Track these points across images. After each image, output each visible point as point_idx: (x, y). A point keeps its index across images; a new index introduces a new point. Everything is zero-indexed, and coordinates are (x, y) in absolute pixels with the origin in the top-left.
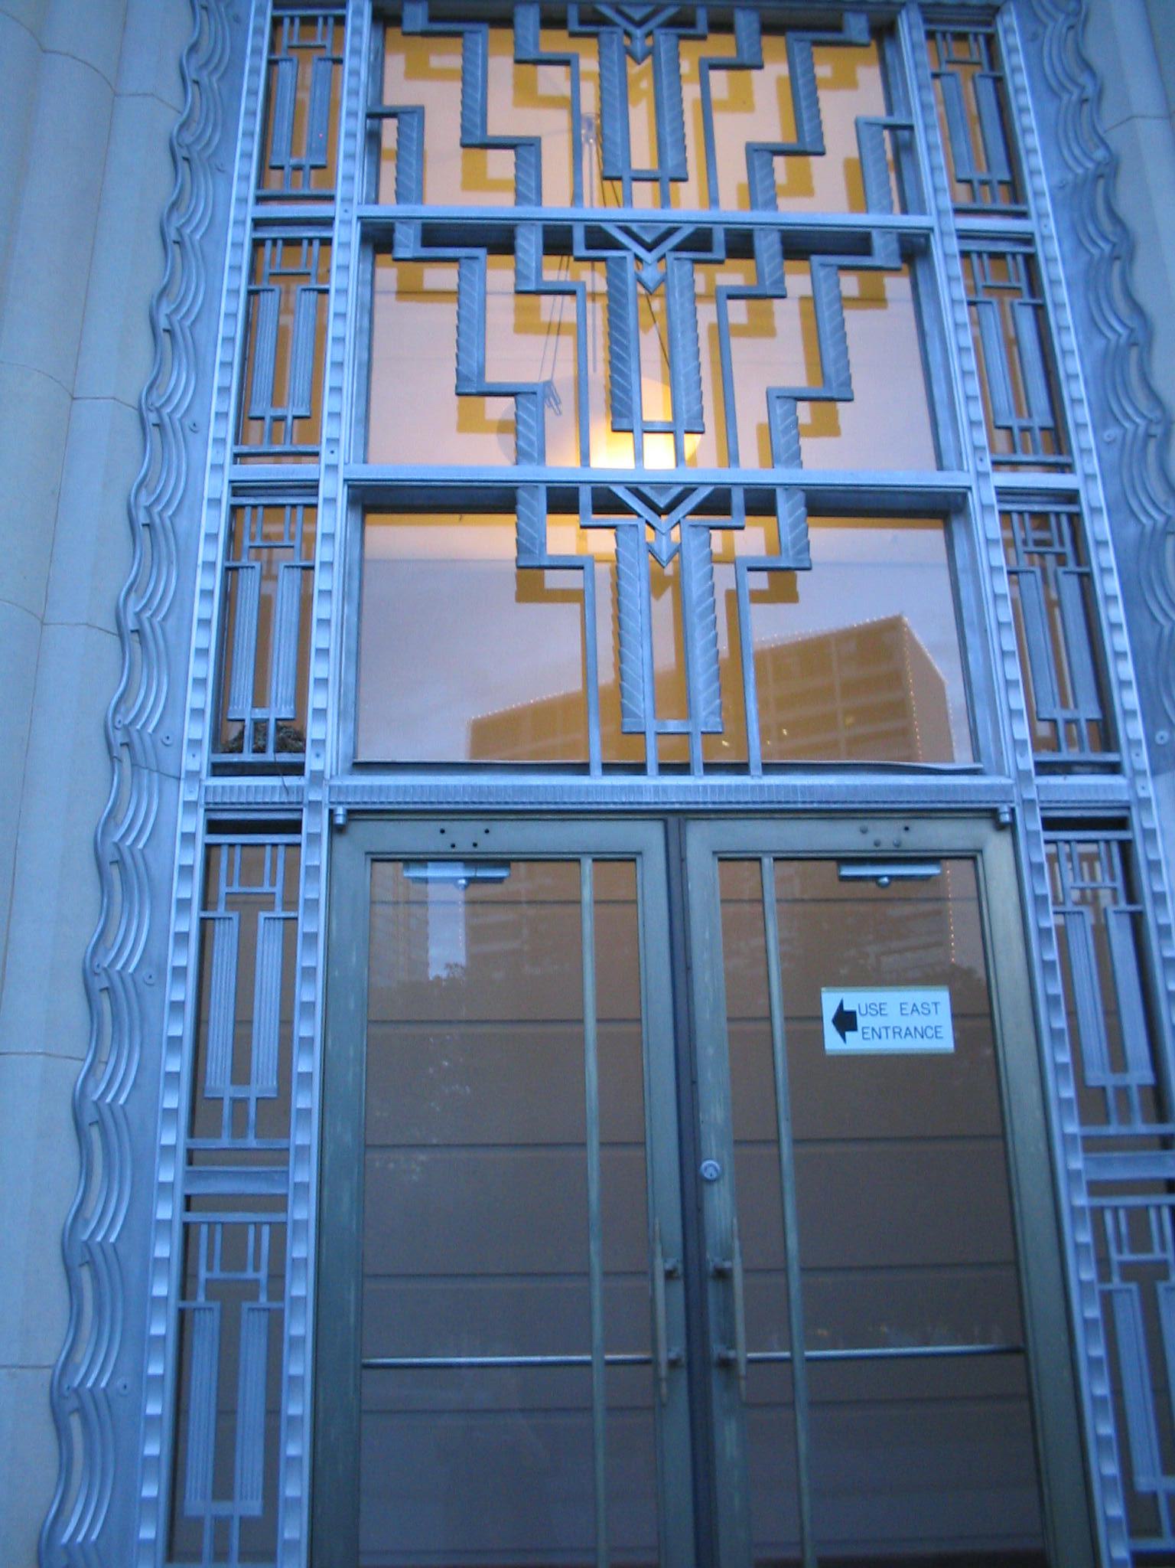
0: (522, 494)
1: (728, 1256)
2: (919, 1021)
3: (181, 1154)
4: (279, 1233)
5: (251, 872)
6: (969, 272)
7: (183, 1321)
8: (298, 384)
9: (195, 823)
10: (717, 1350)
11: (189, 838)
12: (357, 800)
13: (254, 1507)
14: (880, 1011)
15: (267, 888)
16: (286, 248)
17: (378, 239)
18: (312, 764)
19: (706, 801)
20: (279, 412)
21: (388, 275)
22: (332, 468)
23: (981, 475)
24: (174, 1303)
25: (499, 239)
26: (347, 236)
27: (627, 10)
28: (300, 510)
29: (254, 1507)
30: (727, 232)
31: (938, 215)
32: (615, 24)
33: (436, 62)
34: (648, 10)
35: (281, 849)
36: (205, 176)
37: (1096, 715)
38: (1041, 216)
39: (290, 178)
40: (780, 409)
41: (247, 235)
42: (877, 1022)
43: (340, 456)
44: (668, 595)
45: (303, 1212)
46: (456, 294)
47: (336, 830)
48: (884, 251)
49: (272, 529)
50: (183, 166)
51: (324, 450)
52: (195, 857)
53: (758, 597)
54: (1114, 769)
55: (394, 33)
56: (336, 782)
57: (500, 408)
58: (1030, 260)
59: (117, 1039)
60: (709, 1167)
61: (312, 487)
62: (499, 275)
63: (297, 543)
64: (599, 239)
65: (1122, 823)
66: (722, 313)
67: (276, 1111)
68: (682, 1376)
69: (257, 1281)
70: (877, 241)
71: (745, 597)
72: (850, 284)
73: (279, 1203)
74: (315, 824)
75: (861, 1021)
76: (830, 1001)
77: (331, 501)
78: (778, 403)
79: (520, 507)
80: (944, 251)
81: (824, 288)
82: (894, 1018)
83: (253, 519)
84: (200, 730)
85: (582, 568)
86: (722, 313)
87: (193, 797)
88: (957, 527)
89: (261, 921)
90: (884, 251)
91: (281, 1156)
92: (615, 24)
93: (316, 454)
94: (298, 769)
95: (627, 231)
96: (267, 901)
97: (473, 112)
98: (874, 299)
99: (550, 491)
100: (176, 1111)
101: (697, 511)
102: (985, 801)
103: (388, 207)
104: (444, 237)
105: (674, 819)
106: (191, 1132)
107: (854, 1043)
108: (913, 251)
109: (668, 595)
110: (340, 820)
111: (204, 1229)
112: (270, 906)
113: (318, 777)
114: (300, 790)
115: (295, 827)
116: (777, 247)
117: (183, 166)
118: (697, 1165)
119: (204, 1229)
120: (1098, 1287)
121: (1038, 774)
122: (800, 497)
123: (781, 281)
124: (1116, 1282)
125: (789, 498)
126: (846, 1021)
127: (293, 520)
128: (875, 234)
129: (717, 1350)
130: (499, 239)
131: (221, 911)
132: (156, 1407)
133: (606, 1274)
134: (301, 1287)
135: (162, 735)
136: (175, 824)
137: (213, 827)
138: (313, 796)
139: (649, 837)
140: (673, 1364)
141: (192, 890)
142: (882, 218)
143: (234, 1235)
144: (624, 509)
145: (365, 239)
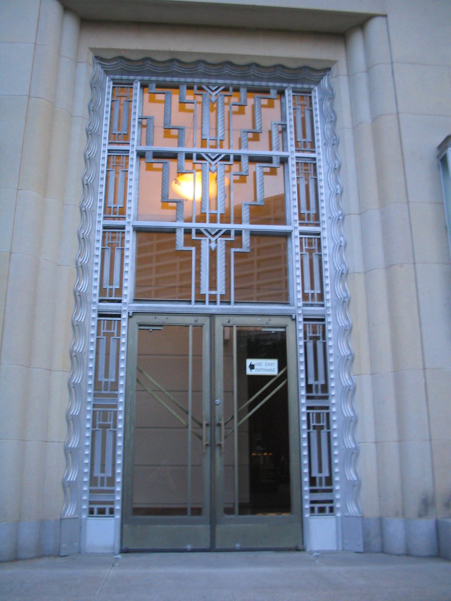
0: (179, 155)
1: (220, 420)
2: (269, 367)
3: (92, 412)
4: (116, 414)
5: (109, 327)
6: (294, 99)
7: (93, 433)
8: (120, 198)
9: (95, 315)
10: (218, 442)
11: (94, 318)
12: (136, 310)
13: (110, 475)
14: (260, 364)
15: (112, 331)
16: (117, 158)
17: (141, 155)
18: (124, 300)
19: (220, 312)
20: (120, 133)
21: (143, 162)
22: (129, 222)
23: (296, 228)
24: (91, 429)
25: (174, 156)
26: (133, 156)
27: (210, 87)
28: (121, 233)
29: (110, 475)
30: (234, 156)
31: (292, 153)
32: (206, 237)
33: (155, 166)
34: (216, 87)
35: (121, 233)
36: (71, 505)
37: (319, 292)
38: (319, 154)
39: (120, 136)
40: (243, 135)
41: (106, 154)
42: (259, 367)
43: (131, 219)
44: (214, 112)
45: (121, 408)
46: (162, 170)
47: (130, 317)
48: (276, 161)
49: (118, 161)
50: (90, 136)
51: (131, 142)
52: (94, 323)
53: (235, 113)
54: (323, 306)
55: (146, 89)
56: (130, 305)
57: (175, 132)
58: (315, 165)
59: (83, 275)
60: (217, 401)
61: (123, 228)
62: (173, 165)
63: (124, 165)
64: (200, 157)
65: (323, 320)
66: (230, 108)
67: (115, 386)
68: (209, 448)
69: (110, 424)
70: (274, 159)
71: (231, 113)
72: (265, 102)
73: (116, 406)
74: (125, 316)
75: (256, 367)
76: (249, 362)
77: (129, 232)
78: (243, 133)
79: (179, 158)
80: (292, 162)
81: (257, 103)
82: (263, 366)
83: (113, 158)
84: (96, 291)
85: (193, 103)
86: (230, 108)
87: (94, 308)
88: (285, 165)
89: (111, 340)
90: (276, 161)
91: (116, 396)
92: (207, 92)
93: (129, 143)
94: (120, 301)
95: (206, 230)
96: (108, 426)
97: (167, 115)
98: (271, 105)
99: (185, 229)
100: (94, 326)
101: (221, 160)
102: (289, 313)
103: (143, 148)
104: (159, 155)
105: (212, 316)
106: (95, 390)
107: (254, 372)
108: (284, 161)
109: (214, 112)
110: (131, 315)
111: (98, 412)
112: (109, 428)
113: (125, 303)
114: (121, 307)
115: (119, 316)
116: (247, 161)
117: (90, 136)
118: (215, 400)
119: (98, 412)
120: (300, 253)
121: (303, 306)
122: (249, 233)
123: (246, 101)
124: (311, 430)
125: (246, 233)
126: (252, 367)
127: (123, 158)
128: (274, 157)
129: (218, 442)
130: (174, 156)
131: (101, 336)
132: (87, 452)
133: (192, 466)
134: (120, 426)
135: (87, 292)
136: (89, 318)
137: (100, 315)
138: (125, 309)
139: (206, 321)
140: (207, 445)
141: (94, 332)
142: (276, 153)
143: (105, 413)
144: (203, 159)
145: (137, 155)
